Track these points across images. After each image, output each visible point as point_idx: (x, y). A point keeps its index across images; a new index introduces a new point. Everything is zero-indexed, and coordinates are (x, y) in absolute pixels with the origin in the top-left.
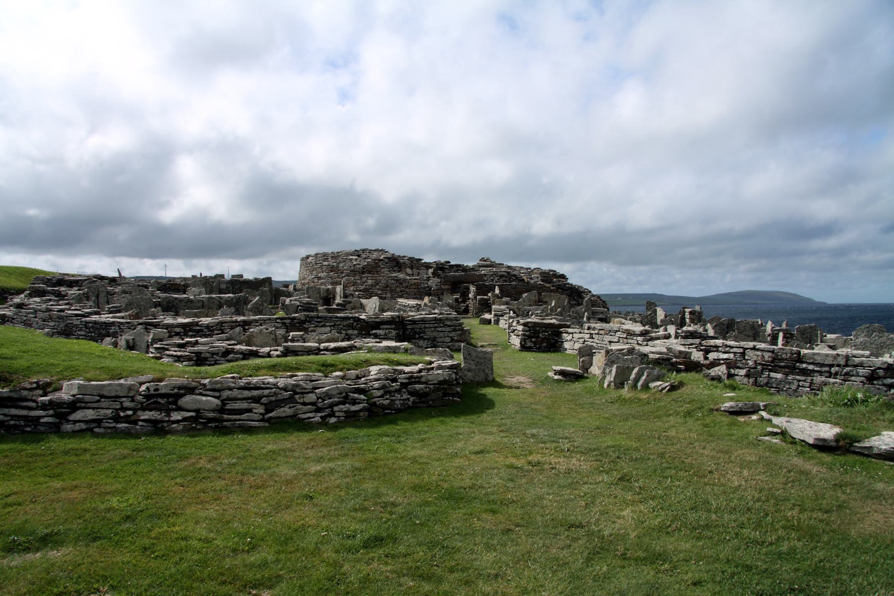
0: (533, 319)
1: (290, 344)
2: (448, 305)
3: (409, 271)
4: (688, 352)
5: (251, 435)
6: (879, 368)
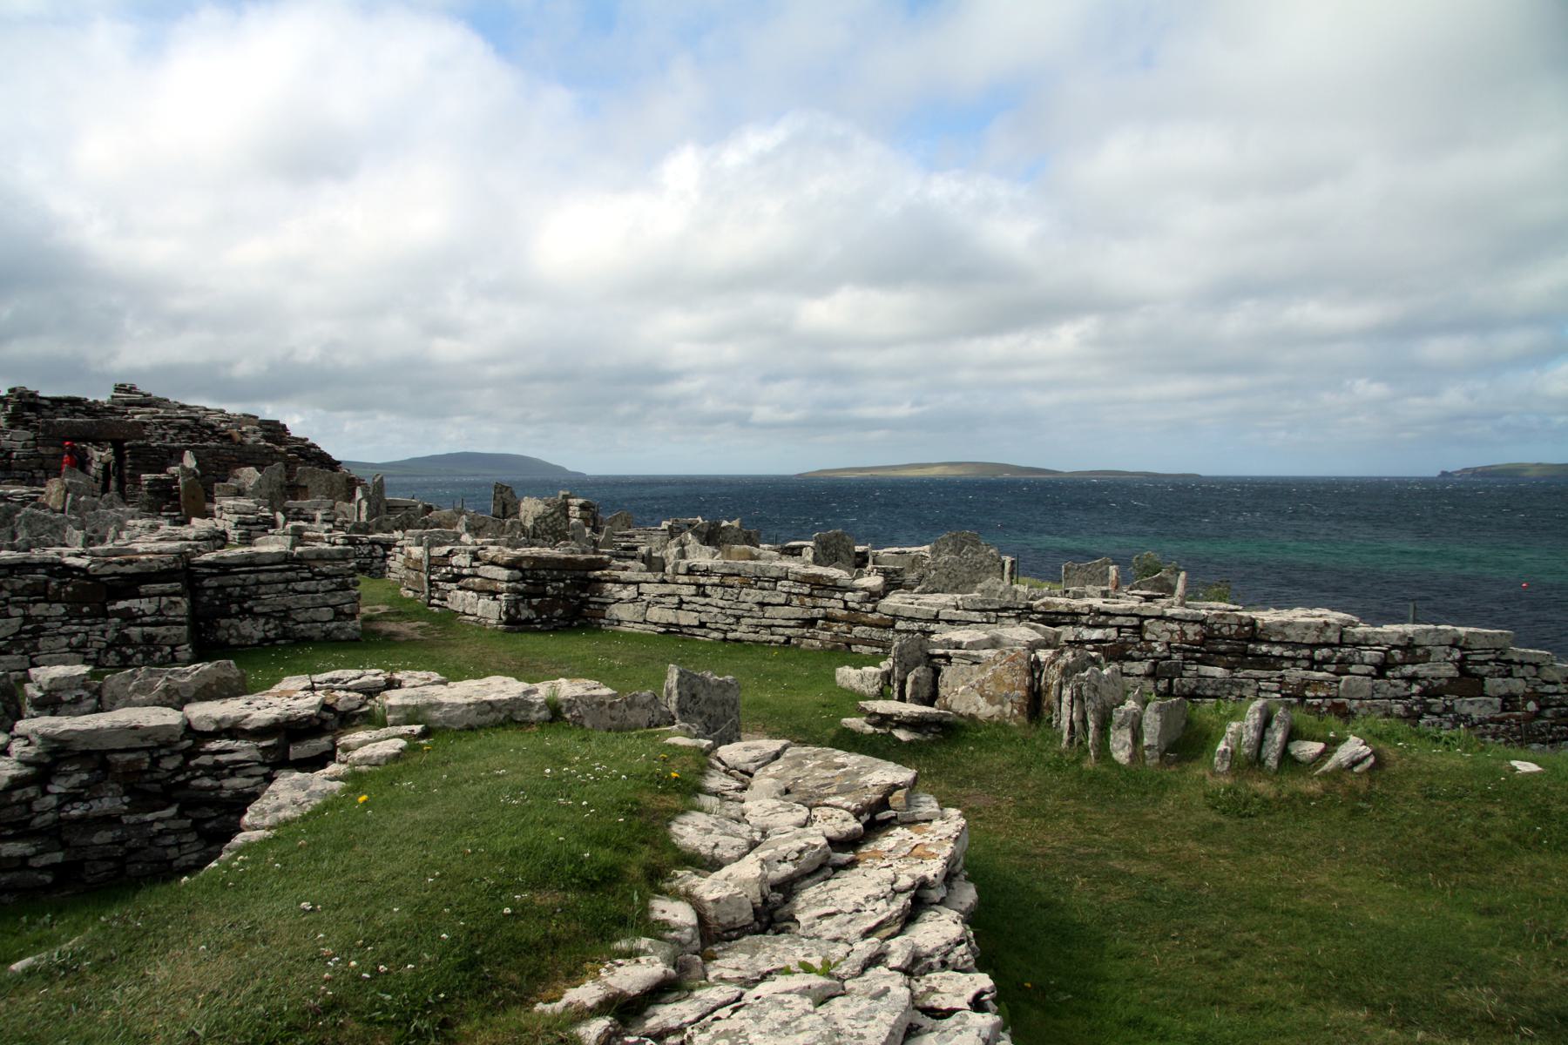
5: (622, 992)
6: (1394, 647)
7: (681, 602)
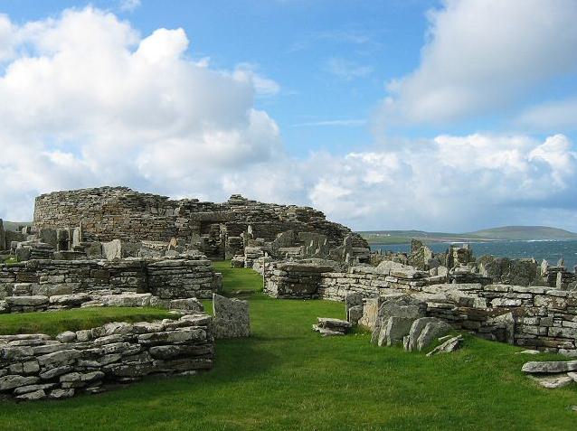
0: (290, 262)
1: (15, 297)
2: (196, 247)
3: (154, 210)
4: (469, 300)
5: (547, 163)
7: (350, 287)
